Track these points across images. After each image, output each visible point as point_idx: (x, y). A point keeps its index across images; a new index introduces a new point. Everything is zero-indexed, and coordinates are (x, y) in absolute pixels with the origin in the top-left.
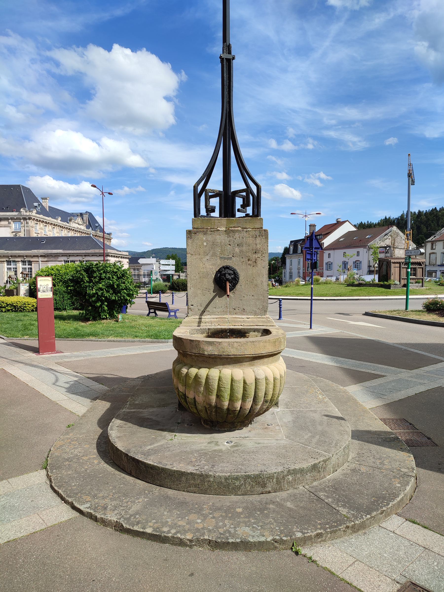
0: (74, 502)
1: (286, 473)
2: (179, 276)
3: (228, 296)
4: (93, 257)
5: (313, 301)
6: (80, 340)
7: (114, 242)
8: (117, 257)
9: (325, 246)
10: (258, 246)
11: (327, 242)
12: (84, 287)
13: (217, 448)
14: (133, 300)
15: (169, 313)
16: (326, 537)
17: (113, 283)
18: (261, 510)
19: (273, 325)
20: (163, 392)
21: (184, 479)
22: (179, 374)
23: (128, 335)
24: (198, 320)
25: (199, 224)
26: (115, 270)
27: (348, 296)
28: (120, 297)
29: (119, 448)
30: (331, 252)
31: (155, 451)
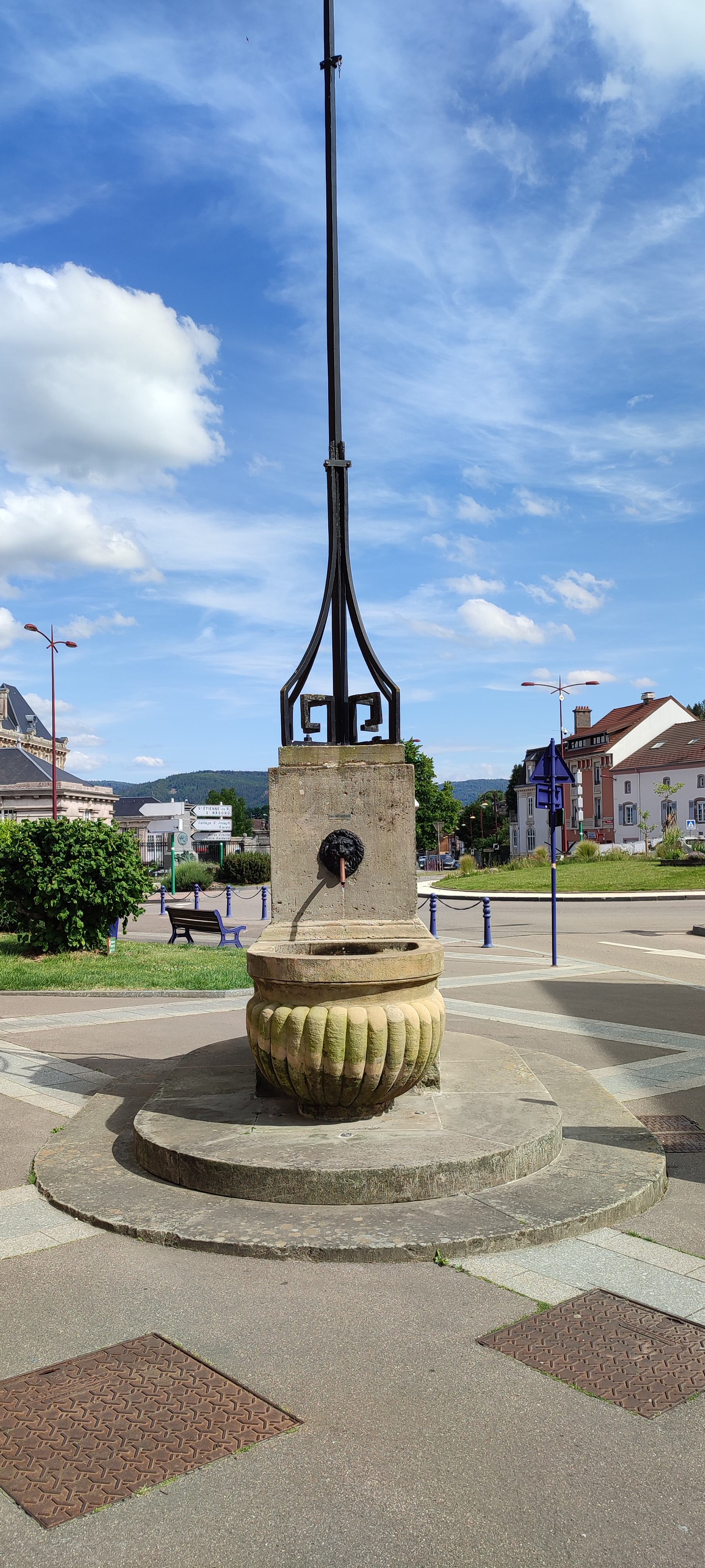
0: (96, 1216)
1: (435, 1169)
2: (242, 845)
3: (343, 884)
4: (25, 801)
5: (558, 904)
6: (30, 994)
7: (71, 762)
8: (83, 799)
9: (616, 761)
10: (397, 795)
11: (621, 751)
12: (31, 876)
13: (324, 1141)
14: (140, 906)
15: (223, 936)
16: (488, 1246)
17: (98, 866)
18: (392, 1219)
19: (426, 936)
20: (223, 1073)
21: (269, 1180)
22: (258, 1020)
23: (136, 981)
24: (290, 930)
25: (290, 758)
26: (102, 837)
27: (661, 890)
28: (113, 898)
29: (160, 1145)
30: (632, 777)
31: (220, 1147)
